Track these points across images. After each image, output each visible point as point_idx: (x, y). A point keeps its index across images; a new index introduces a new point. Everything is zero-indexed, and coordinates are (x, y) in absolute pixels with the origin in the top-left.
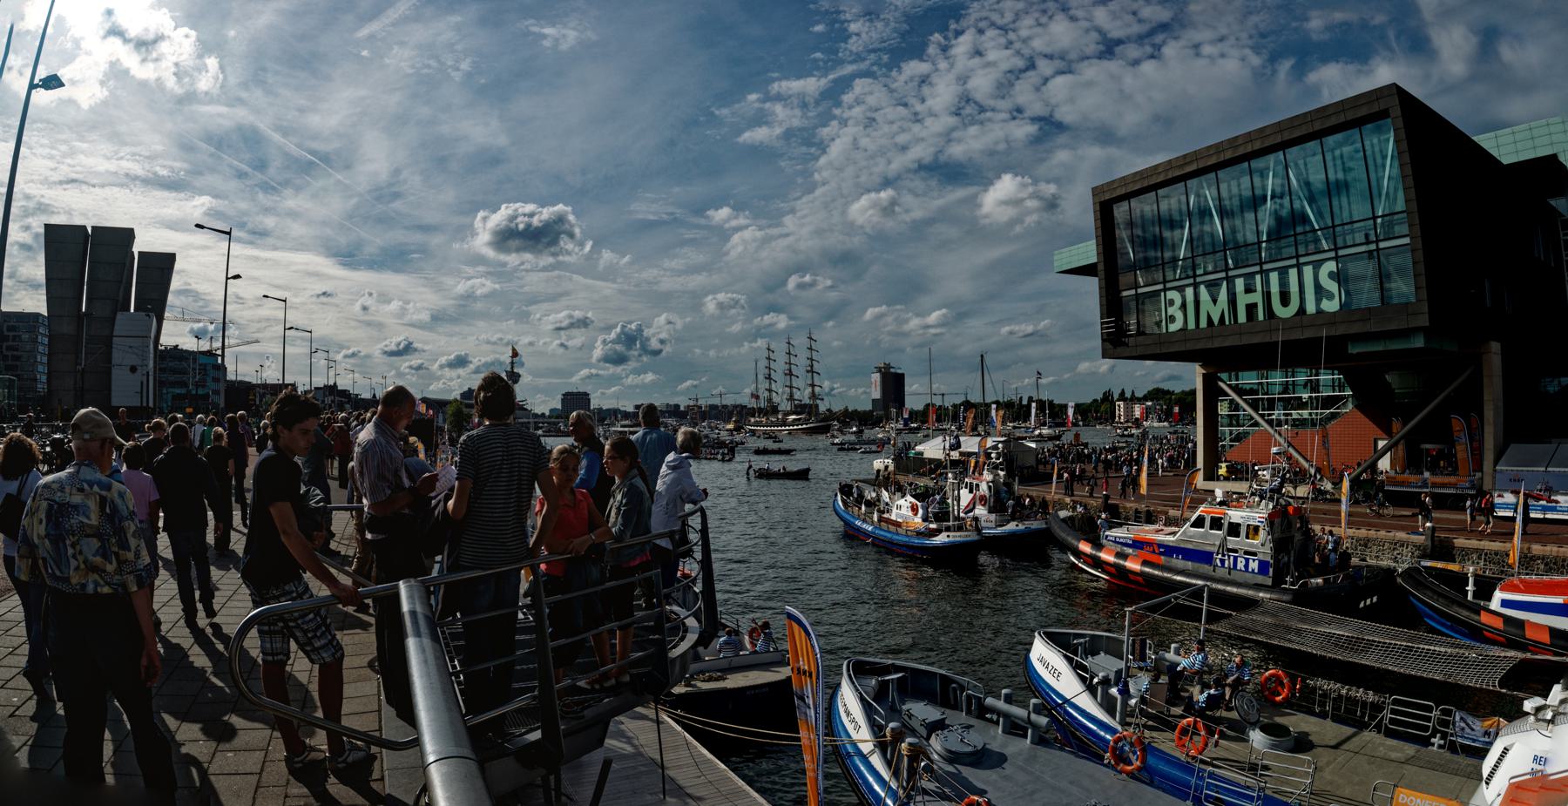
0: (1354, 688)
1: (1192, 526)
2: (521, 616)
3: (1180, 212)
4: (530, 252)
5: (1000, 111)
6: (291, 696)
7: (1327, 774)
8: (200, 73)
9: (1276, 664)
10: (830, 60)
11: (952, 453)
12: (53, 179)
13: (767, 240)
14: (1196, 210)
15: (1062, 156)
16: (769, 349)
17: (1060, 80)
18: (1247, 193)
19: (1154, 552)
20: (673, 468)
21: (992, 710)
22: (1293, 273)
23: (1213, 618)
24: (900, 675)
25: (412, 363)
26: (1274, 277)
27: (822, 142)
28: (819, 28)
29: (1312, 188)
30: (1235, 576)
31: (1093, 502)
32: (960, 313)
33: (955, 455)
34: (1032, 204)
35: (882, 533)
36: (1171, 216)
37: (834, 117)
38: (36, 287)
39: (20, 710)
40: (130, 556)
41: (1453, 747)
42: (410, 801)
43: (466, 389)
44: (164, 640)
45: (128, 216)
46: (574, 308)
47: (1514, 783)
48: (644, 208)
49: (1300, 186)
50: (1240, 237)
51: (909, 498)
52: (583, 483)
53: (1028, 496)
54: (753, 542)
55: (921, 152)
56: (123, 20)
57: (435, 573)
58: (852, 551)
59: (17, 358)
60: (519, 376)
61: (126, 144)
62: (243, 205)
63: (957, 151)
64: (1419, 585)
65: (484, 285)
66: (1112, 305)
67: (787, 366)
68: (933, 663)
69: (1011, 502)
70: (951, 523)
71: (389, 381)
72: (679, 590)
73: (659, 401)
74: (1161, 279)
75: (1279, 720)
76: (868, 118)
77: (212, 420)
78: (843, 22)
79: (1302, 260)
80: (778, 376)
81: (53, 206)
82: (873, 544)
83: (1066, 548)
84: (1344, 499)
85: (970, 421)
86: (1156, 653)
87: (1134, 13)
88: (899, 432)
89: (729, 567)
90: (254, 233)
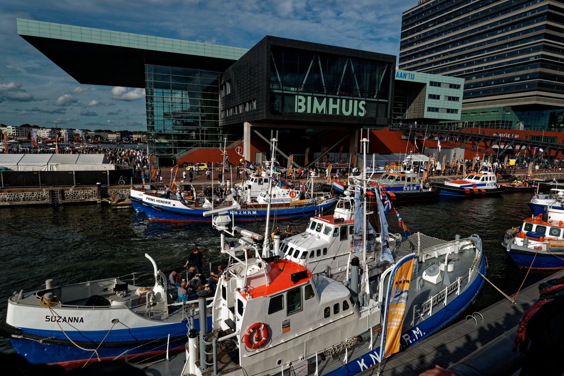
26: (344, 101)
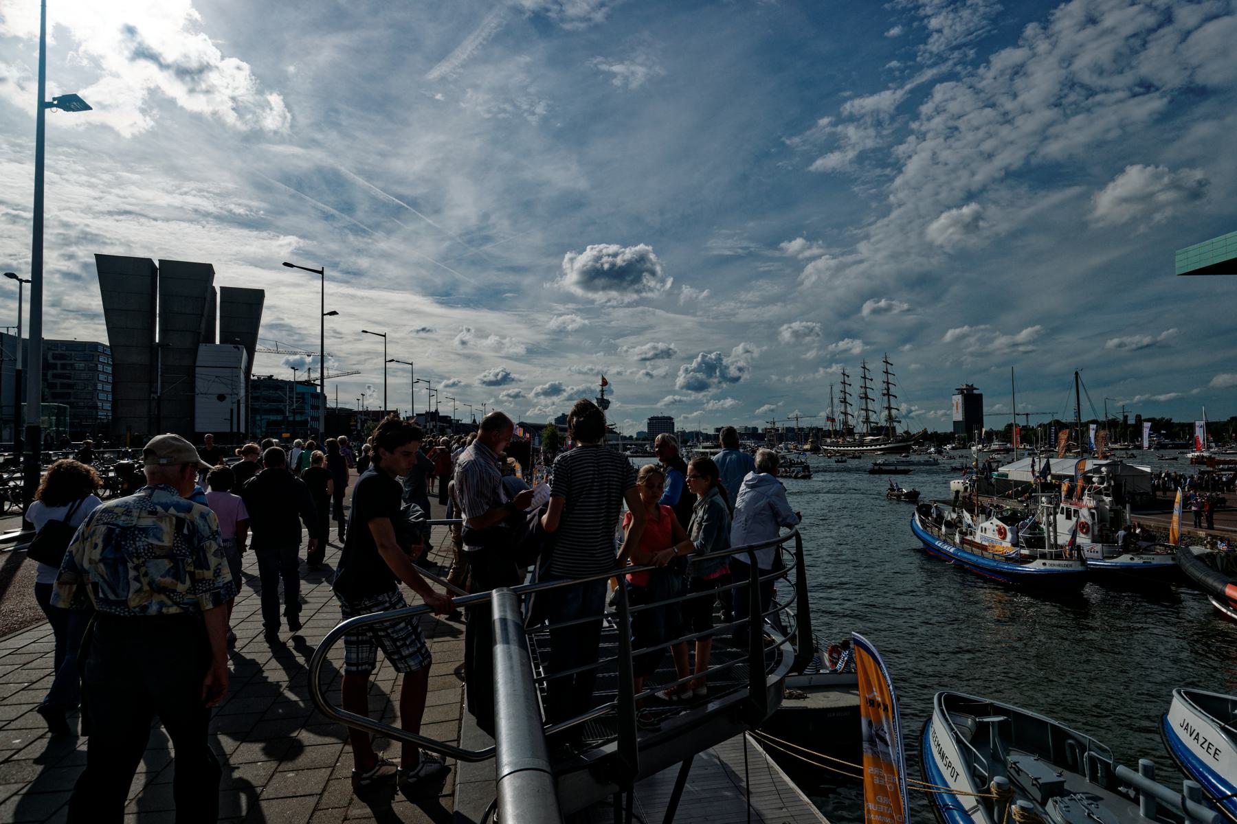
2: (605, 624)
4: (615, 290)
5: (1117, 90)
6: (370, 707)
8: (264, 110)
10: (906, 68)
12: (97, 209)
13: (840, 268)
15: (1203, 130)
16: (844, 374)
20: (752, 487)
21: (1128, 784)
24: (1001, 718)
25: (510, 392)
27: (898, 160)
28: (895, 31)
32: (1053, 327)
35: (966, 555)
37: (912, 132)
38: (93, 316)
39: (22, 753)
40: (209, 574)
42: (477, 819)
43: (560, 414)
44: (238, 658)
45: (203, 252)
48: (721, 244)
51: (996, 521)
52: (668, 499)
53: (1139, 526)
55: (1010, 157)
56: (151, 38)
57: (527, 583)
59: (70, 386)
60: (608, 402)
61: (190, 179)
62: (334, 246)
63: (1054, 149)
65: (574, 321)
67: (863, 390)
69: (1121, 533)
70: (1047, 550)
71: (488, 408)
73: (738, 424)
76: (950, 128)
77: (311, 444)
78: (922, 19)
80: (854, 400)
81: (105, 237)
90: (348, 272)
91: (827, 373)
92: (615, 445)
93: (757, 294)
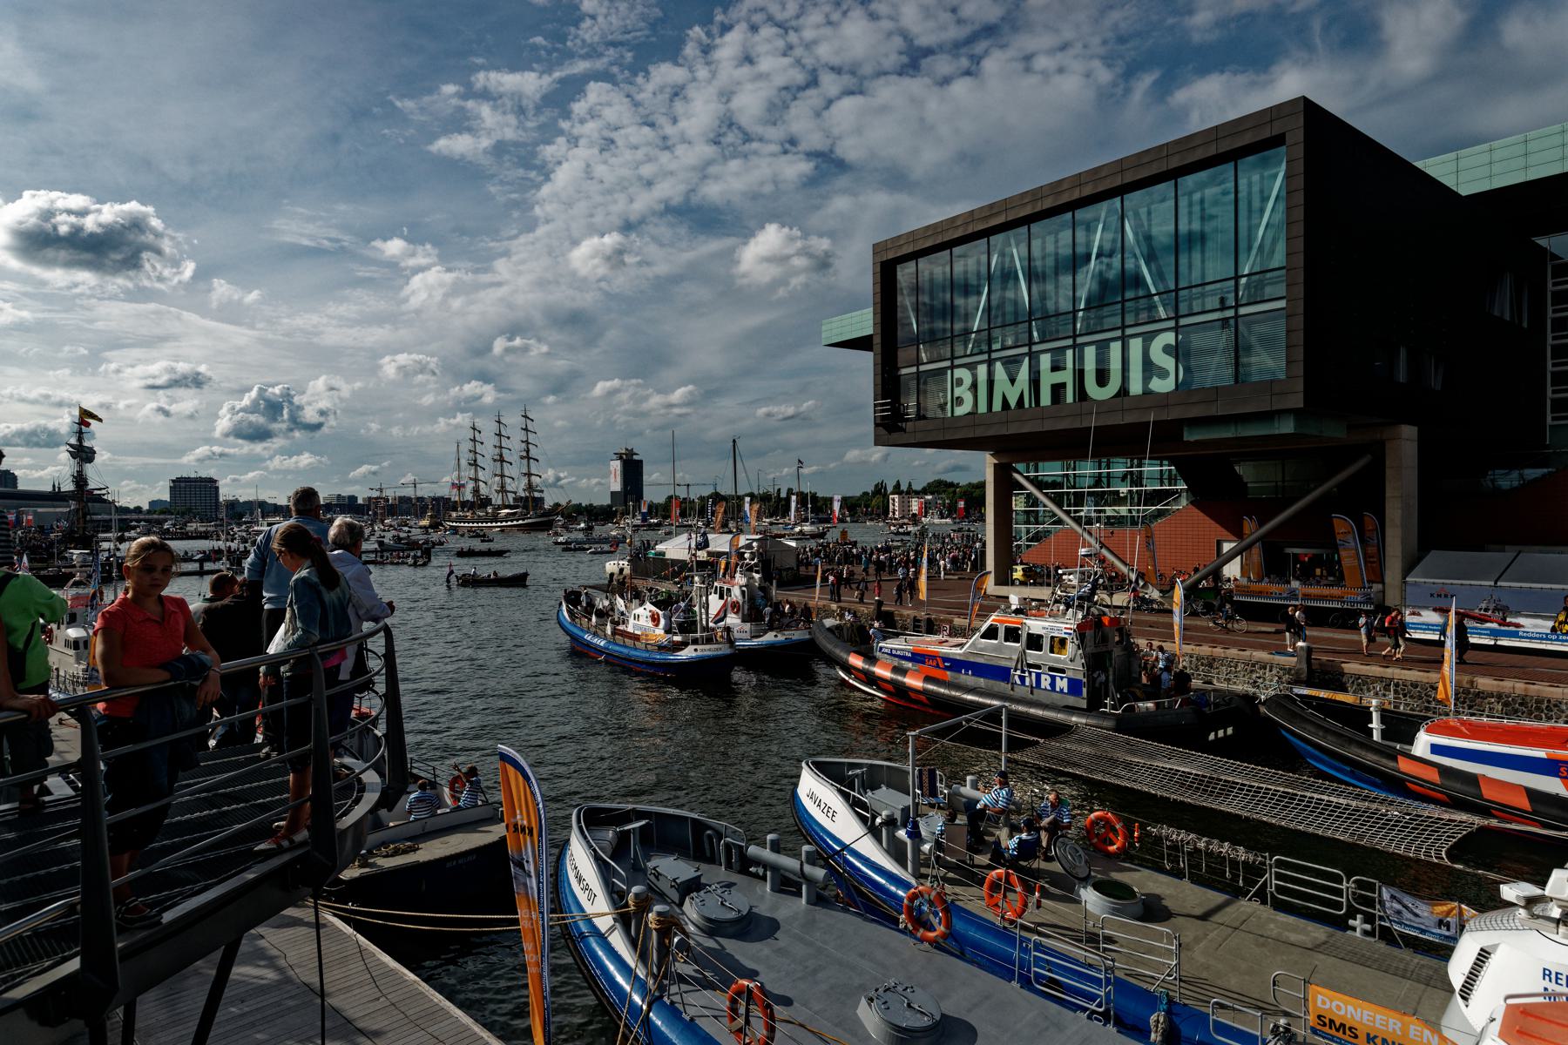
0: (1216, 841)
1: (984, 636)
3: (978, 274)
5: (769, 142)
7: (1198, 954)
9: (1102, 804)
11: (699, 553)
14: (998, 273)
15: (841, 203)
16: (474, 429)
17: (848, 103)
18: (1066, 251)
19: (938, 666)
21: (758, 862)
22: (1116, 348)
23: (1015, 745)
24: (643, 822)
26: (1090, 353)
29: (1154, 243)
30: (1038, 696)
31: (863, 609)
32: (710, 390)
33: (702, 555)
34: (799, 262)
35: (617, 648)
36: (966, 279)
37: (561, 132)
41: (1387, 935)
46: (177, 359)
47: (1517, 1006)
49: (1138, 242)
50: (1050, 305)
51: (649, 606)
53: (788, 602)
54: (455, 666)
55: (669, 190)
58: (580, 671)
63: (713, 191)
64: (1294, 716)
66: (889, 385)
67: (498, 450)
68: (683, 805)
69: (768, 609)
70: (699, 635)
72: (352, 736)
74: (948, 355)
75: (1116, 876)
76: (605, 139)
79: (1129, 331)
82: (607, 662)
83: (833, 662)
84: (1176, 609)
85: (720, 516)
86: (949, 787)
87: (954, 10)
88: (636, 528)
89: (424, 699)
91: (449, 425)
92: (105, 521)
93: (354, 308)
